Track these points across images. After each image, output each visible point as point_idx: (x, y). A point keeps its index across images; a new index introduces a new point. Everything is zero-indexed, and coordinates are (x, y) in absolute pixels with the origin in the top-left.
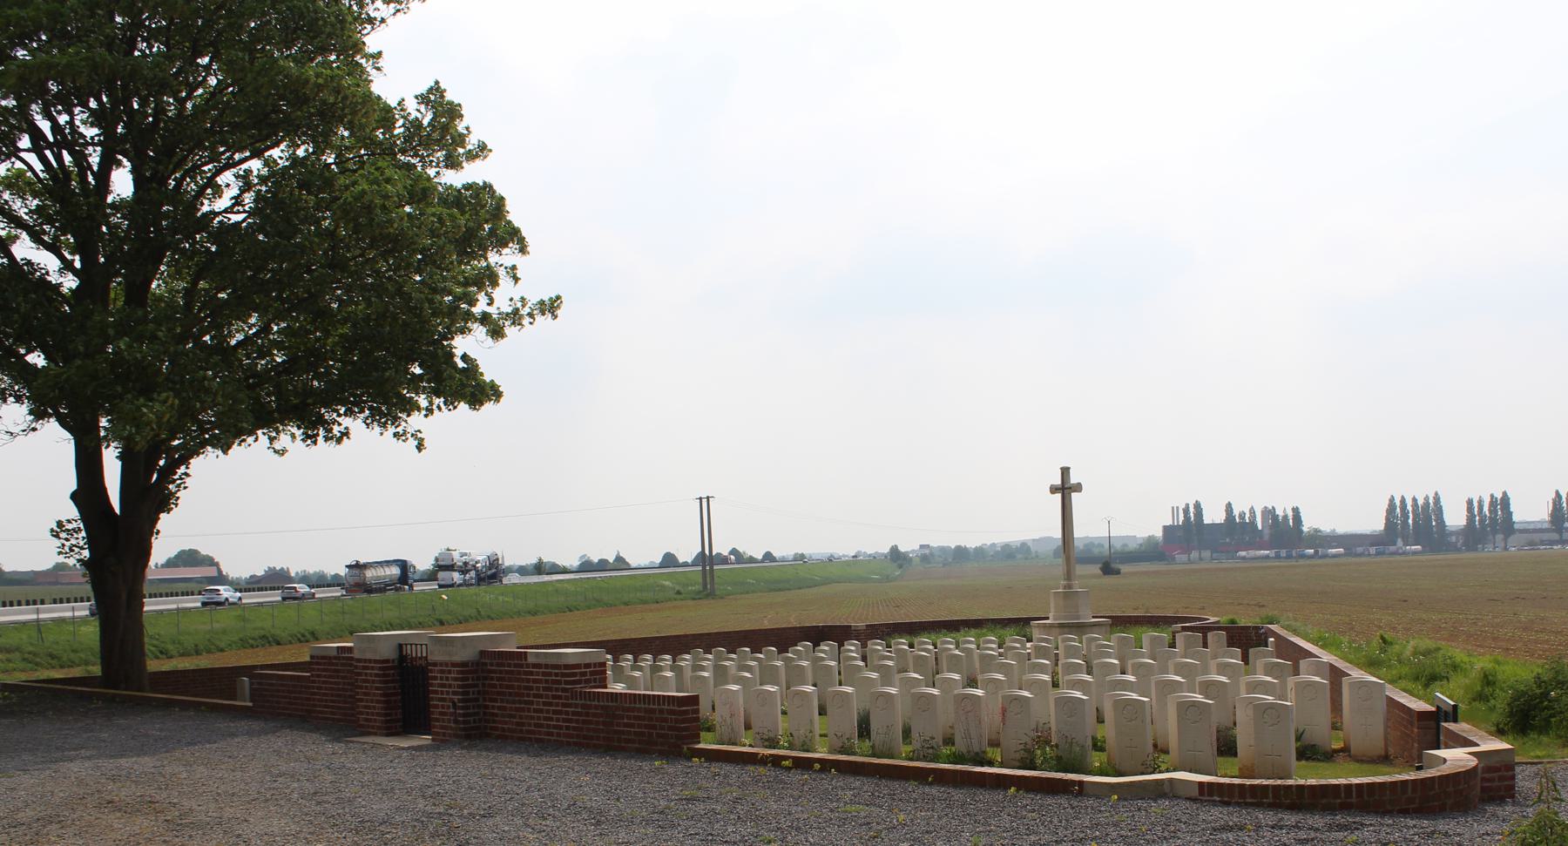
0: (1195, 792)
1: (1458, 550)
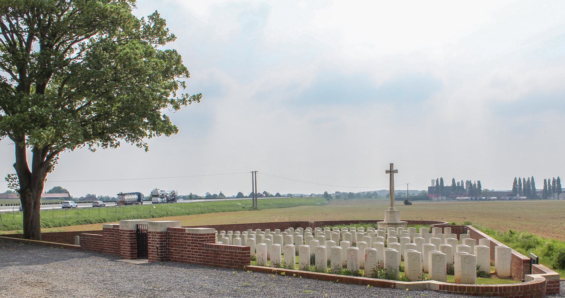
1: (540, 199)
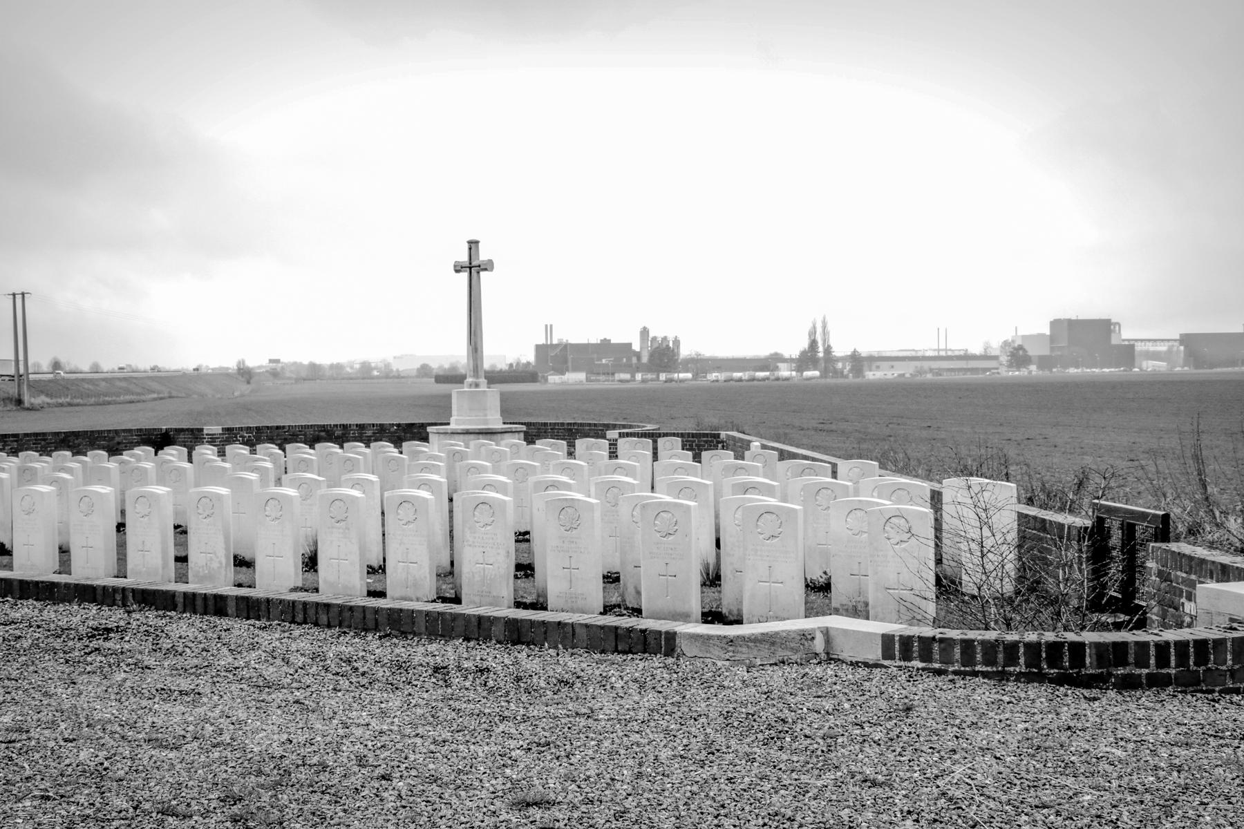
0: (874, 653)
